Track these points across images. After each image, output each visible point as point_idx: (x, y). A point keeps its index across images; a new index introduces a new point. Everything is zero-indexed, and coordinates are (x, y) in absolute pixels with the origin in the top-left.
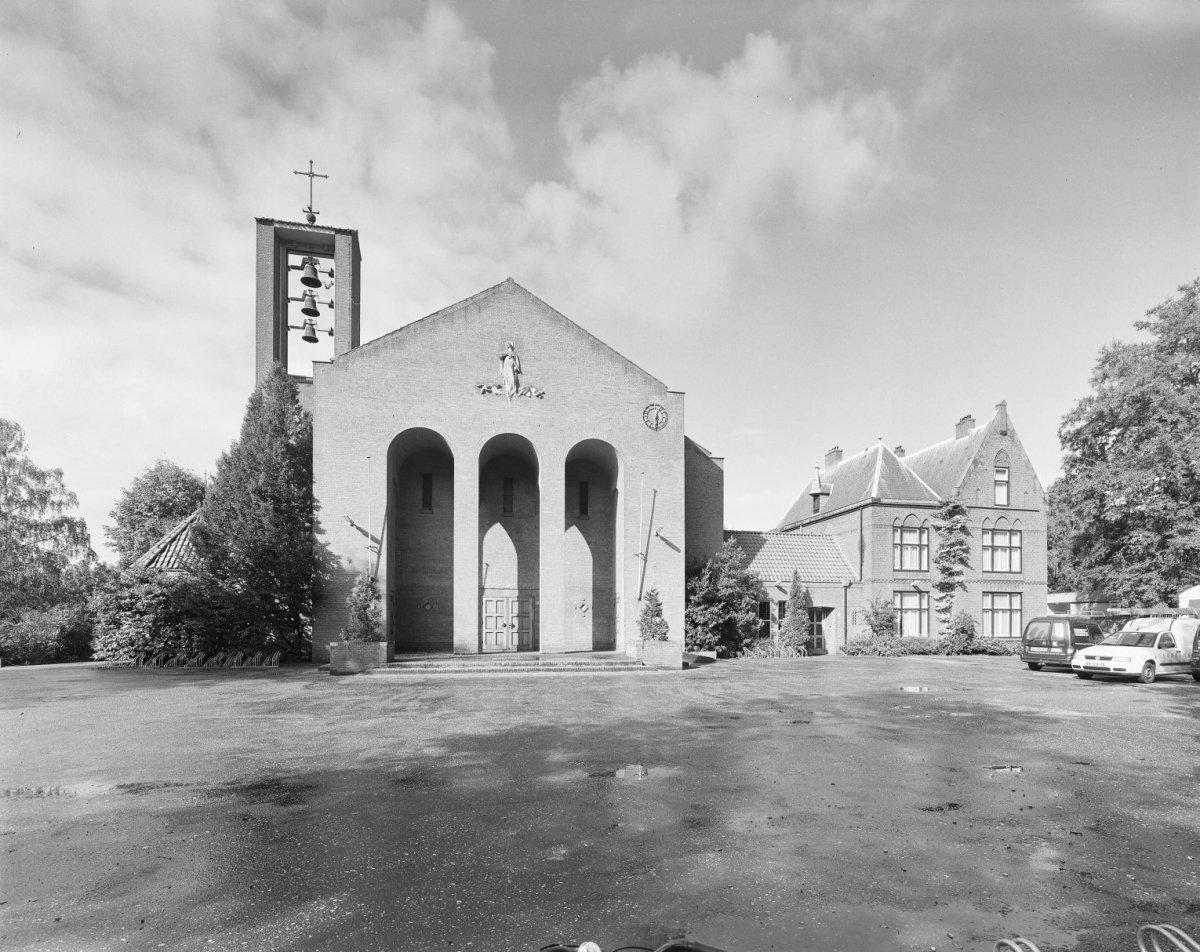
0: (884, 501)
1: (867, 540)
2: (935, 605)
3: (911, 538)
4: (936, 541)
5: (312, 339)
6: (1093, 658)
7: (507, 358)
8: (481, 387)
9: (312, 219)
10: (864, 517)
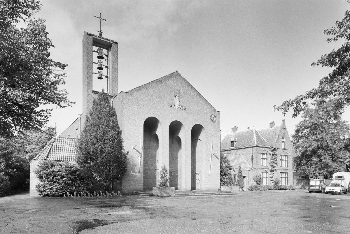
0: (259, 146)
1: (254, 157)
2: (269, 176)
3: (264, 157)
4: (270, 157)
5: (100, 78)
6: (330, 189)
7: (177, 97)
8: (169, 105)
9: (101, 35)
10: (253, 150)
